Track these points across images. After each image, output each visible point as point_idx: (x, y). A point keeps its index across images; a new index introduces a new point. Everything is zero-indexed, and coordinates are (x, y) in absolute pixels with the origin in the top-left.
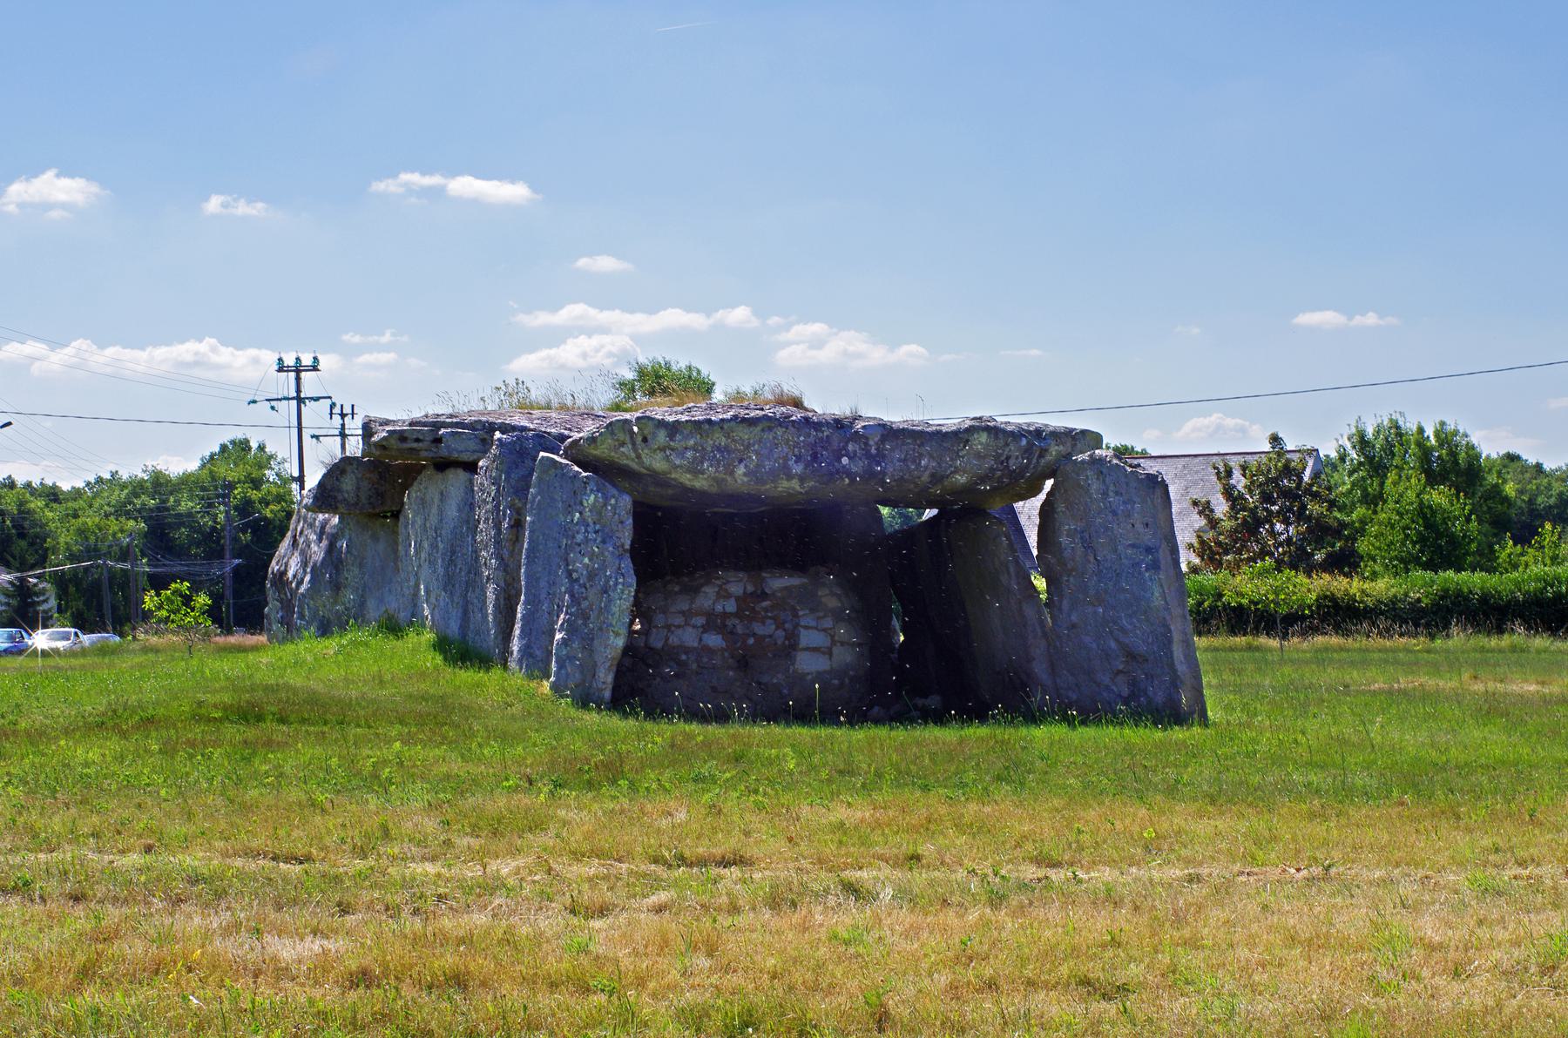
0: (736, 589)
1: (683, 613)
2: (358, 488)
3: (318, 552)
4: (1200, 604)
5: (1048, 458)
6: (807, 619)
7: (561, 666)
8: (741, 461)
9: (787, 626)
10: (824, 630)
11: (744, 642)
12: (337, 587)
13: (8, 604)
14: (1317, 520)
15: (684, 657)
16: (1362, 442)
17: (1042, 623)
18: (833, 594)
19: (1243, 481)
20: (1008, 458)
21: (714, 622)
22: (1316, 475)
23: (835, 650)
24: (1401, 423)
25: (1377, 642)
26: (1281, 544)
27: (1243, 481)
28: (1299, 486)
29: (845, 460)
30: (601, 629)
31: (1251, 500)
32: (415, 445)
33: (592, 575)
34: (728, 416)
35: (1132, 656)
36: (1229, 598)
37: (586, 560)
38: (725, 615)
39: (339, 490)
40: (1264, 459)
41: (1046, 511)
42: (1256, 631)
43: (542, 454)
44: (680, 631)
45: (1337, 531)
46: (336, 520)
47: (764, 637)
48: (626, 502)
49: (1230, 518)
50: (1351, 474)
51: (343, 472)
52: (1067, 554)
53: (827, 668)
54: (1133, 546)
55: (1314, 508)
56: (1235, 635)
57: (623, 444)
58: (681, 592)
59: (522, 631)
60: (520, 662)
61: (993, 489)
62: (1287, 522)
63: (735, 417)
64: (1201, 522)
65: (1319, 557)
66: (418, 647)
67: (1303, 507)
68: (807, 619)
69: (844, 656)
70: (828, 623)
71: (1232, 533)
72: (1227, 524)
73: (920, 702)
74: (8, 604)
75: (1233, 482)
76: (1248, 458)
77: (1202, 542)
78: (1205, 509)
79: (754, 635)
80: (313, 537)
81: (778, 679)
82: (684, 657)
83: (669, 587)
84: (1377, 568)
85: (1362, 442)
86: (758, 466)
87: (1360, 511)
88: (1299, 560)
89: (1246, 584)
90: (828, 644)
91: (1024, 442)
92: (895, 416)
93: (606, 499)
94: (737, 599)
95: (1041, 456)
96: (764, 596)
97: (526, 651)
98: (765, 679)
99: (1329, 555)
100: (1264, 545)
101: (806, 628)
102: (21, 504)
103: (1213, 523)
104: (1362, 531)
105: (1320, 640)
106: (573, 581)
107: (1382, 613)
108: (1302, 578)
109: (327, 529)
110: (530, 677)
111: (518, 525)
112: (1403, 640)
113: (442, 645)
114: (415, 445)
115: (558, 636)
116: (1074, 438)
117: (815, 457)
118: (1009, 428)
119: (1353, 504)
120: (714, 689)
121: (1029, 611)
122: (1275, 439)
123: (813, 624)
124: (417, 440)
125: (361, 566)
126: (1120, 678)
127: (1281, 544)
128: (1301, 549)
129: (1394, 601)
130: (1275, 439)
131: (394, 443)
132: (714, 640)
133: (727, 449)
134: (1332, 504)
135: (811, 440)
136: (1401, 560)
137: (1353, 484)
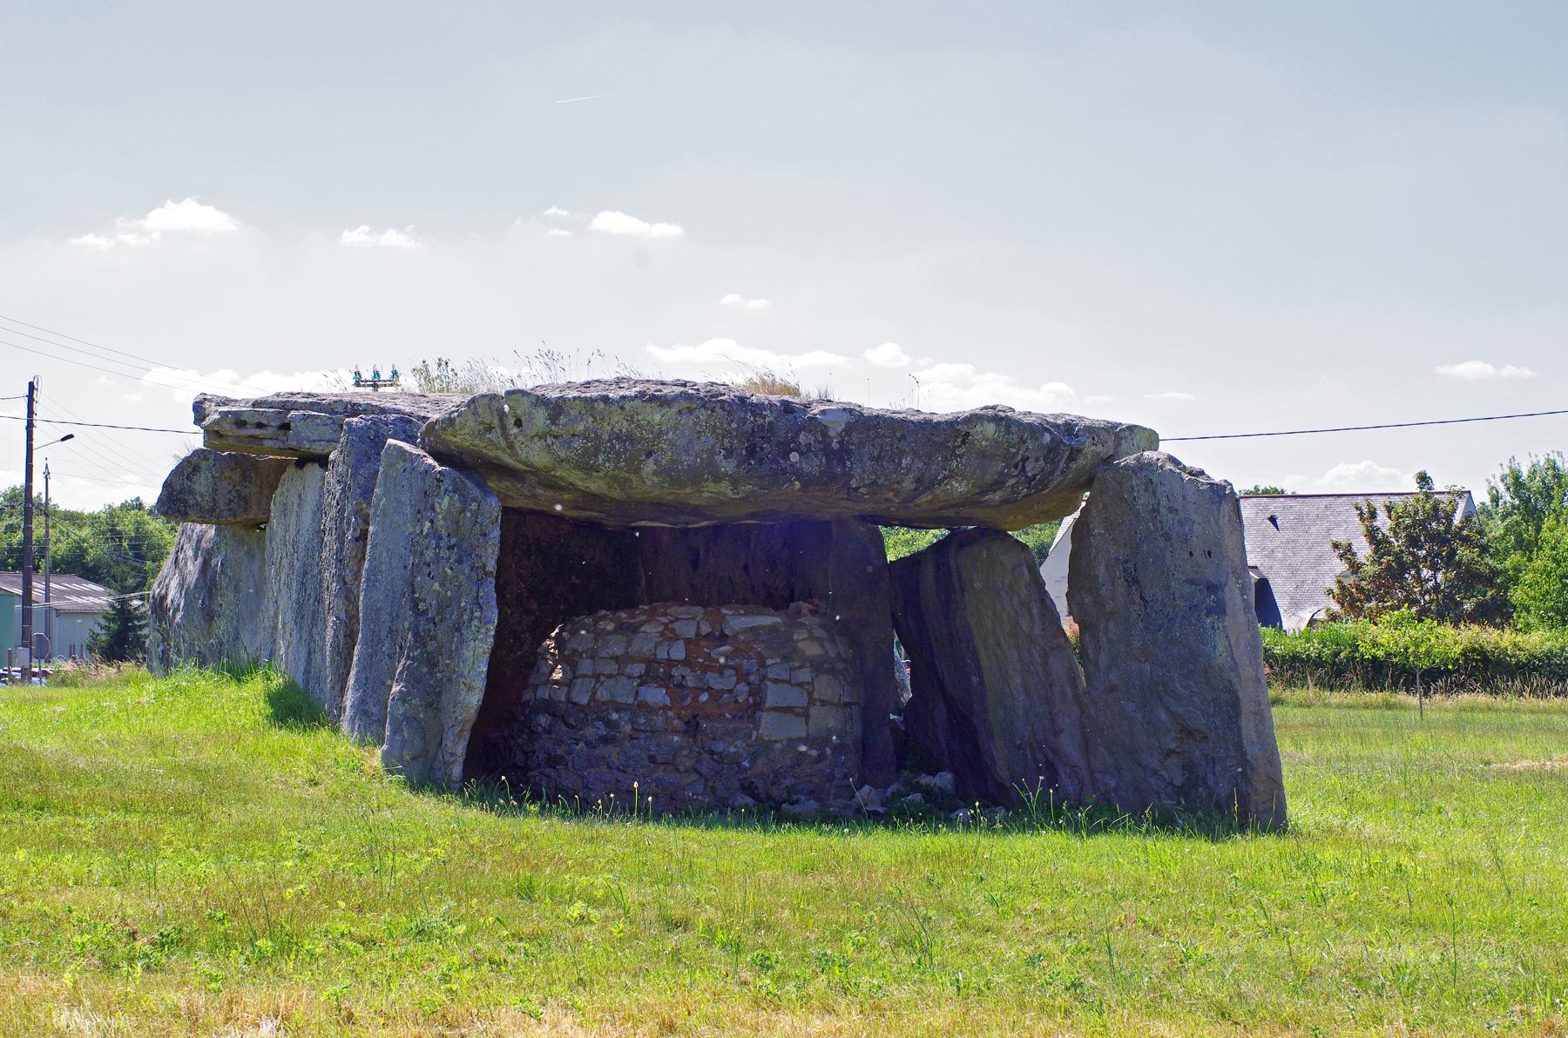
1: (616, 658)
2: (215, 491)
3: (193, 569)
4: (1336, 654)
5: (1081, 461)
7: (394, 732)
8: (649, 454)
9: (752, 678)
10: (800, 685)
11: (695, 698)
12: (210, 616)
13: (108, 628)
14: (1468, 566)
15: (615, 716)
16: (1517, 484)
17: (1073, 680)
18: (812, 638)
19: (1389, 523)
20: (1025, 459)
21: (656, 672)
22: (1467, 518)
24: (1559, 464)
25: (1529, 701)
26: (1427, 592)
27: (1389, 523)
28: (1447, 532)
29: (794, 457)
30: (450, 680)
31: (1397, 544)
32: (257, 432)
33: (443, 606)
34: (633, 392)
35: (1187, 732)
36: (1366, 651)
37: (436, 586)
38: (671, 663)
39: (191, 492)
40: (1411, 500)
41: (1079, 531)
42: (1395, 687)
43: (391, 441)
44: (612, 682)
45: (1490, 578)
46: (212, 532)
47: (722, 692)
48: (493, 506)
49: (1373, 562)
50: (1504, 518)
51: (196, 469)
52: (1104, 592)
54: (1192, 582)
55: (1464, 553)
56: (1371, 690)
57: (490, 429)
58: (614, 631)
59: (357, 680)
60: (352, 720)
61: (1004, 502)
62: (1435, 568)
63: (642, 394)
64: (1342, 567)
65: (1468, 606)
66: (248, 699)
67: (1453, 553)
69: (826, 719)
70: (805, 675)
71: (1376, 577)
72: (1371, 569)
73: (925, 780)
74: (108, 628)
75: (1377, 523)
76: (1393, 499)
77: (1343, 588)
78: (1346, 552)
79: (709, 689)
80: (190, 553)
81: (735, 747)
82: (615, 716)
83: (601, 624)
84: (1531, 620)
85: (1517, 484)
86: (673, 461)
87: (1515, 558)
88: (1446, 610)
89: (1384, 634)
90: (805, 703)
91: (1047, 437)
92: (876, 401)
93: (465, 501)
94: (687, 641)
95: (1072, 458)
96: (723, 638)
97: (362, 711)
98: (719, 747)
99: (1479, 605)
100: (1410, 592)
101: (776, 681)
102: (139, 525)
103: (1355, 568)
104: (1515, 580)
105: (1465, 698)
106: (419, 614)
107: (1535, 669)
108: (1447, 630)
109: (203, 544)
110: (362, 743)
111: (362, 537)
112: (1559, 700)
113: (275, 699)
114: (257, 432)
115: (396, 689)
116: (1117, 435)
117: (752, 451)
118: (1027, 420)
119: (1507, 550)
120: (652, 759)
121: (1057, 666)
122: (1423, 479)
123: (786, 676)
124: (260, 425)
125: (237, 590)
126: (1173, 761)
127: (1427, 592)
128: (1449, 597)
129: (1549, 655)
130: (1423, 479)
131: (228, 428)
132: (656, 695)
133: (630, 438)
134: (1484, 549)
135: (748, 427)
136: (1558, 611)
137: (1507, 530)
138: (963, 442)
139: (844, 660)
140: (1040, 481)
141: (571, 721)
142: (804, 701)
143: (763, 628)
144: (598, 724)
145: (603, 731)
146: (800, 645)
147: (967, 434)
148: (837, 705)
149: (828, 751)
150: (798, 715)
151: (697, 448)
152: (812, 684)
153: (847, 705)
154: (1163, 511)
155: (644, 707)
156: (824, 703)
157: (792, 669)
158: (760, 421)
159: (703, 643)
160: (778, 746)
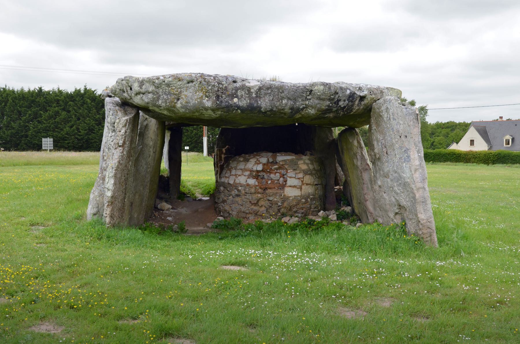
0: (264, 160)
6: (291, 173)
10: (299, 179)
18: (305, 163)
23: (303, 187)
38: (258, 171)
53: (300, 194)
68: (291, 173)
69: (308, 190)
70: (301, 175)
82: (240, 188)
94: (264, 164)
98: (271, 198)
101: (290, 177)
126: (398, 216)
132: (252, 182)
138: (310, 94)
139: (315, 170)
140: (348, 109)
141: (228, 189)
142: (300, 184)
143: (288, 160)
144: (235, 190)
145: (237, 193)
146: (300, 166)
147: (312, 91)
148: (313, 185)
149: (309, 200)
150: (298, 188)
151: (196, 97)
152: (303, 178)
153: (316, 185)
154: (392, 120)
155: (248, 185)
156: (307, 184)
157: (296, 174)
158: (221, 86)
159: (269, 165)
160: (291, 198)
